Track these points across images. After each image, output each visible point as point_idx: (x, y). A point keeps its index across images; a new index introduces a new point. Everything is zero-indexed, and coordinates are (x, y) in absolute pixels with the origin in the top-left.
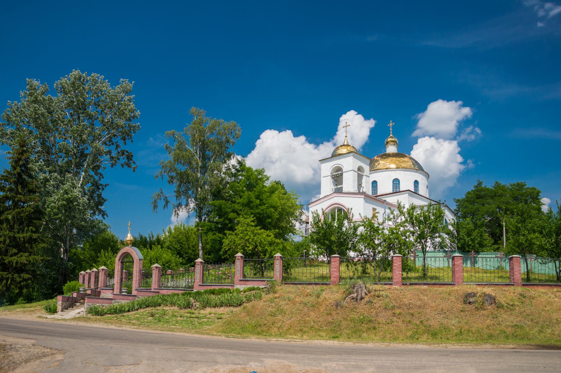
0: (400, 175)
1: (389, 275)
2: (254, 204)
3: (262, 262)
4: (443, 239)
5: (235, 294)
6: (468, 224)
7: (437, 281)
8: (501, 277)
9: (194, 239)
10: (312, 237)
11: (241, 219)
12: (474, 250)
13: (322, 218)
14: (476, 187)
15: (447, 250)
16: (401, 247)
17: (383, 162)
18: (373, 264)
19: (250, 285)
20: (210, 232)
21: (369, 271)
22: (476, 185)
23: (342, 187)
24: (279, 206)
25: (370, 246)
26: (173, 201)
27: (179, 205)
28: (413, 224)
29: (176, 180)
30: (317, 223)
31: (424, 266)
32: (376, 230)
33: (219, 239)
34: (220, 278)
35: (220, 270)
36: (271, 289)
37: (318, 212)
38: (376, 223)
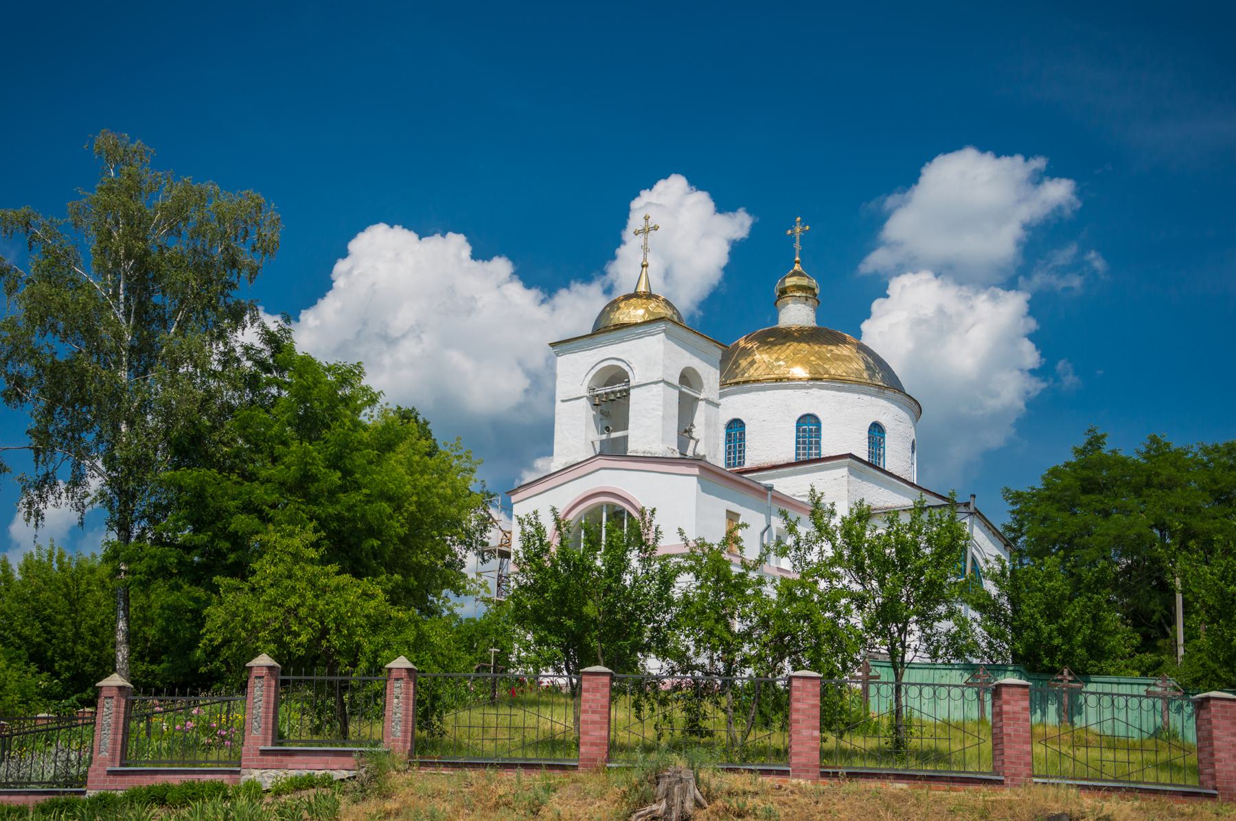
0: (820, 402)
1: (777, 740)
2: (323, 485)
3: (345, 687)
4: (963, 624)
5: (242, 802)
6: (1050, 576)
7: (941, 767)
8: (1169, 765)
9: (98, 604)
10: (519, 605)
11: (271, 535)
12: (1072, 665)
13: (552, 537)
14: (1083, 452)
15: (975, 661)
16: (817, 645)
17: (765, 357)
18: (724, 702)
19: (297, 769)
20: (160, 581)
21: (708, 724)
22: (1081, 446)
23: (626, 438)
24: (408, 496)
25: (715, 641)
26: (25, 466)
27: (46, 483)
28: (860, 568)
29: (33, 392)
30: (537, 555)
31: (898, 712)
32: (735, 586)
33: (191, 605)
34: (189, 746)
35: (189, 717)
36: (372, 784)
37: (542, 520)
38: (737, 561)
